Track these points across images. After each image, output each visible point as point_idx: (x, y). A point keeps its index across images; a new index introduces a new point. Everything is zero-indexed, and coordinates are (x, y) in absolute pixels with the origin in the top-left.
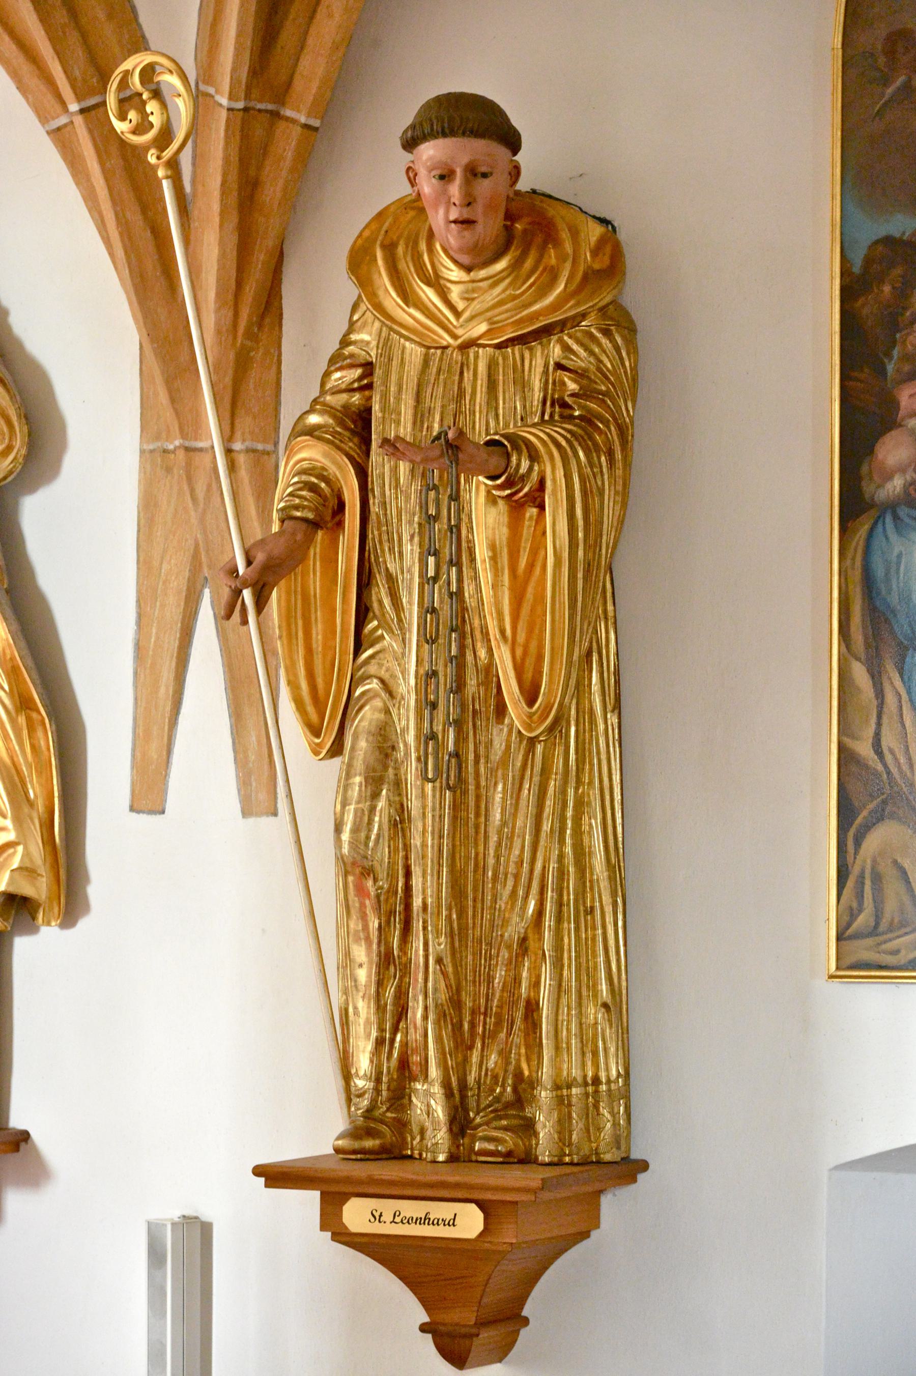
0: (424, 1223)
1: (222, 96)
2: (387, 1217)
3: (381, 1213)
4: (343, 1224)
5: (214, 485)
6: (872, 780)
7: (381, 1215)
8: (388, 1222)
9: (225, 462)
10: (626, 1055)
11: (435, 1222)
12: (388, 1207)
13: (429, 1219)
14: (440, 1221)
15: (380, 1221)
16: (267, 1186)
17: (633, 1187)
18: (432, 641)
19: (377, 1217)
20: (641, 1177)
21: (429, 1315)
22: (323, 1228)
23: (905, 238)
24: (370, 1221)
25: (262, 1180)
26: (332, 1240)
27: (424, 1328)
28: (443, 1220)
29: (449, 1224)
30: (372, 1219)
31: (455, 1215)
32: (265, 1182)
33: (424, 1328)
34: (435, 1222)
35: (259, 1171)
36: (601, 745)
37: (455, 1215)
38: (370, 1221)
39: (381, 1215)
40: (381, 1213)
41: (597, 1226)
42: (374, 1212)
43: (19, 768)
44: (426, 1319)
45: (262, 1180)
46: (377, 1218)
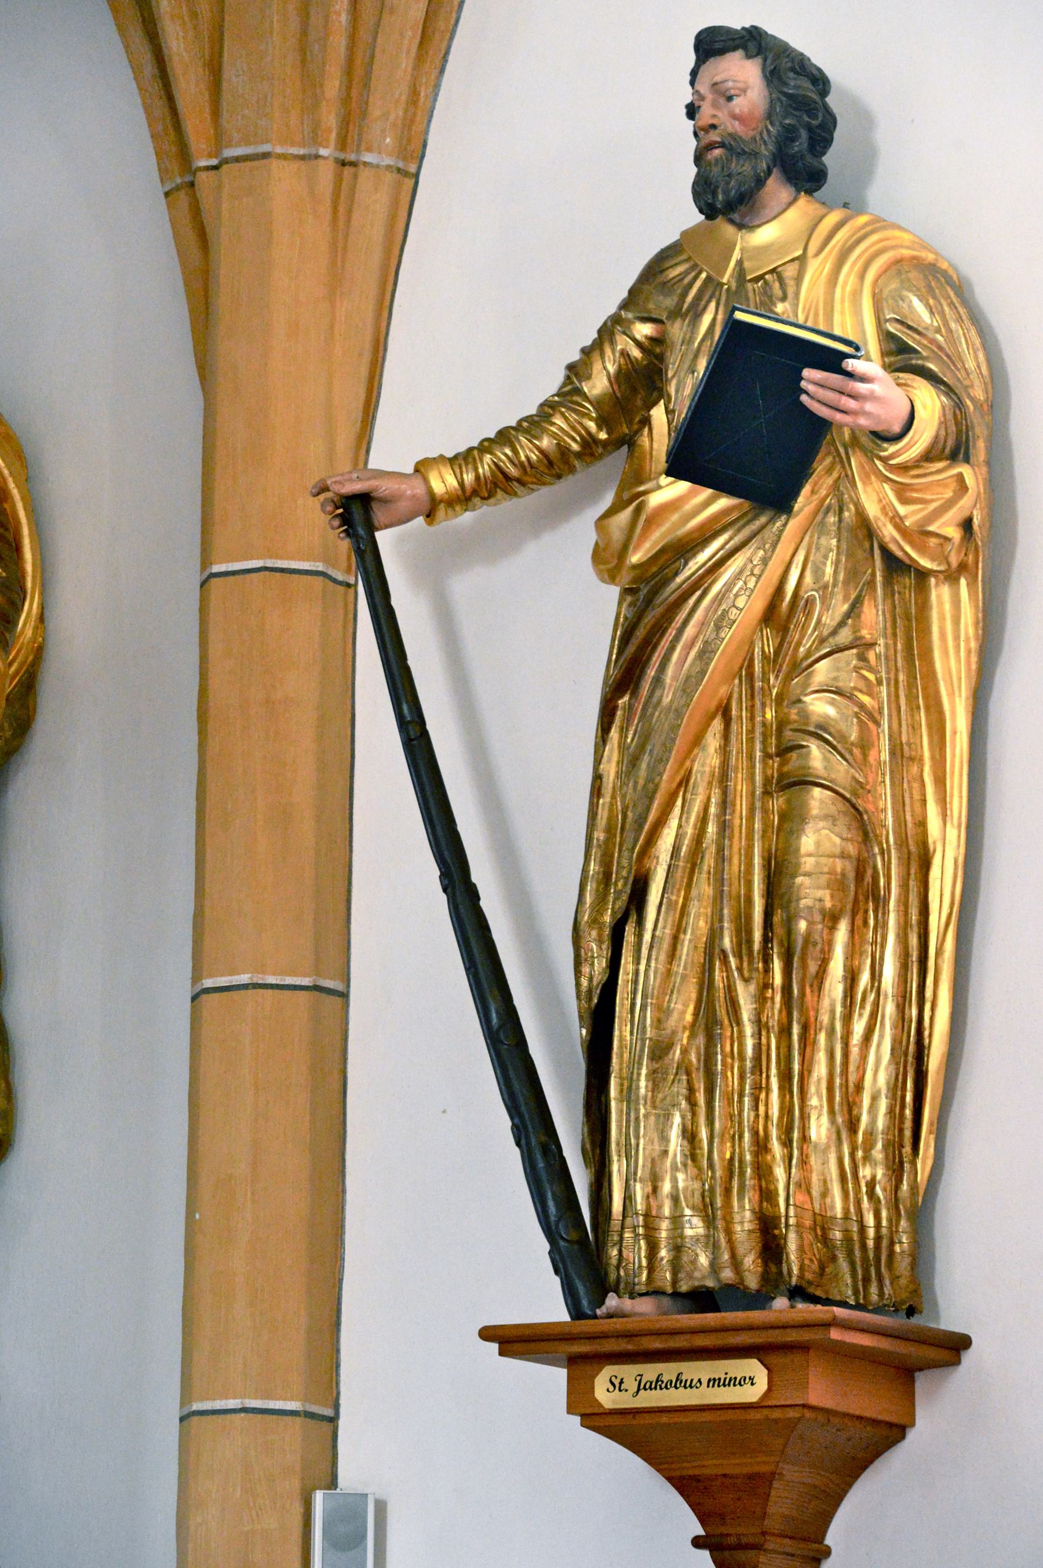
1: (868, 359)
2: (631, 1385)
3: (622, 1379)
6: (769, 483)
7: (621, 1382)
9: (970, 724)
11: (647, 1386)
14: (747, 1380)
15: (620, 1390)
16: (501, 1353)
22: (571, 1410)
24: (608, 1390)
25: (495, 1347)
26: (582, 1425)
27: (698, 1543)
28: (750, 1378)
29: (666, 1387)
30: (611, 1388)
33: (698, 1543)
34: (647, 1386)
35: (487, 1334)
38: (608, 1390)
39: (621, 1382)
40: (622, 1379)
42: (613, 1379)
44: (701, 1532)
45: (495, 1347)
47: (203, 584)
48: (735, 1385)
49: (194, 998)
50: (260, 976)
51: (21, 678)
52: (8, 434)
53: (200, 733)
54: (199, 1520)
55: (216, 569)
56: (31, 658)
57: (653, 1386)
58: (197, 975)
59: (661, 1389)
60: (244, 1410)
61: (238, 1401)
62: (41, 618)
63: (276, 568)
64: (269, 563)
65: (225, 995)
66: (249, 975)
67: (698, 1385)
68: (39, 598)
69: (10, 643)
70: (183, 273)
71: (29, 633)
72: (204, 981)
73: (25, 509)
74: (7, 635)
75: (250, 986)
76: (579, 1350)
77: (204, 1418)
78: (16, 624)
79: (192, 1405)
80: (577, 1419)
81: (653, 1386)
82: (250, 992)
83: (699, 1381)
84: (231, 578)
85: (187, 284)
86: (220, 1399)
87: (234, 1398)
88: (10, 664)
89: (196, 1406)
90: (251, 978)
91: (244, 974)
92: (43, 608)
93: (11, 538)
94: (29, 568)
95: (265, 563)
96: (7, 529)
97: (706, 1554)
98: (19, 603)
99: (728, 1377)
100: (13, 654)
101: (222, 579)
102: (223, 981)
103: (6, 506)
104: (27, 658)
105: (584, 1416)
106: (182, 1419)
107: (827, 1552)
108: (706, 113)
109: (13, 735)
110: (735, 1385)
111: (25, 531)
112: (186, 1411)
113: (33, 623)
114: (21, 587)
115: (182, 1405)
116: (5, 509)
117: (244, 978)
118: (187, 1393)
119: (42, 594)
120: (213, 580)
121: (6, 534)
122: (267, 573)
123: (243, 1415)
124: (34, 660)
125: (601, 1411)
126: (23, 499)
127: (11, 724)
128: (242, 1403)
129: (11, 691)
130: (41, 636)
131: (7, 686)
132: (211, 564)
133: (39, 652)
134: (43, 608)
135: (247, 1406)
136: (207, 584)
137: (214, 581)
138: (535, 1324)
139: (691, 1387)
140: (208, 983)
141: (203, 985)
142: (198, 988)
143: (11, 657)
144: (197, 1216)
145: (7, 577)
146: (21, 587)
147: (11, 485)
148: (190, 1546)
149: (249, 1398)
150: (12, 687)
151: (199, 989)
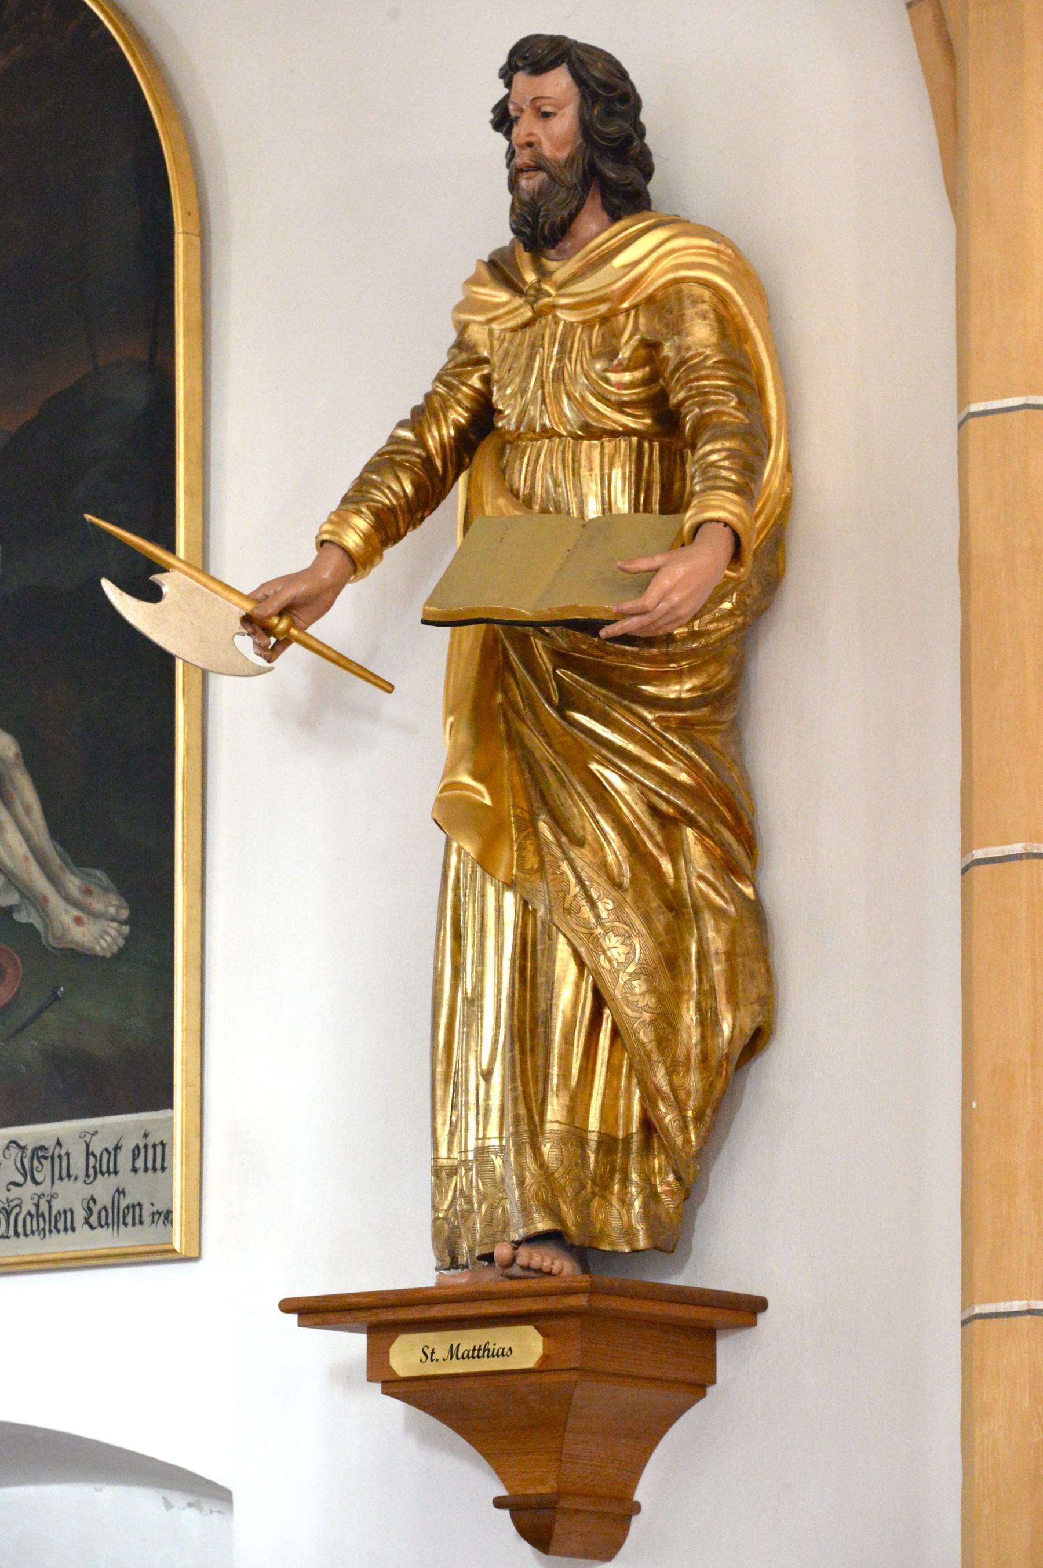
0: (483, 1356)
2: (442, 1352)
4: (391, 1368)
5: (646, 792)
7: (433, 1353)
8: (441, 1360)
10: (369, 676)
12: (469, 1339)
13: (489, 1350)
15: (432, 1360)
17: (753, 1330)
18: (562, 873)
19: (429, 1355)
20: (761, 1318)
21: (508, 1488)
23: (125, 914)
27: (499, 1503)
31: (389, 688)
32: (299, 1320)
33: (499, 1503)
35: (287, 1306)
36: (592, 807)
37: (389, 688)
39: (433, 1353)
41: (713, 1382)
43: (692, 533)
44: (503, 1492)
45: (294, 1317)
46: (429, 1355)
47: (961, 425)
48: (488, 1357)
49: (965, 870)
50: (1035, 845)
51: (768, 532)
52: (747, 271)
53: (962, 588)
54: (985, 1430)
55: (974, 408)
56: (778, 510)
57: (470, 1355)
58: (967, 846)
59: (488, 1357)
60: (1030, 1312)
61: (1024, 1302)
62: (789, 467)
63: (1039, 405)
64: (1032, 400)
65: (998, 865)
66: (1023, 844)
67: (509, 1353)
68: (785, 445)
69: (755, 493)
70: (929, 91)
71: (776, 482)
72: (974, 852)
73: (767, 351)
74: (752, 486)
75: (1024, 857)
76: (389, 1318)
77: (988, 1321)
78: (761, 474)
79: (973, 1308)
80: (378, 1386)
81: (470, 1355)
82: (1024, 862)
83: (510, 1349)
84: (990, 417)
85: (933, 99)
86: (1004, 1300)
87: (1020, 1299)
88: (757, 517)
89: (978, 1309)
90: (1025, 848)
91: (1016, 843)
92: (789, 455)
93: (753, 381)
94: (773, 413)
95: (1027, 400)
96: (749, 373)
97: (506, 1514)
98: (764, 451)
99: (497, 1348)
100: (760, 505)
101: (981, 418)
102: (995, 852)
103: (747, 347)
104: (773, 513)
105: (384, 1382)
106: (964, 1323)
107: (636, 1508)
108: (526, 126)
109: (760, 593)
110: (458, 1358)
111: (768, 373)
112: (967, 1314)
113: (779, 472)
114: (765, 434)
115: (963, 1309)
116: (746, 351)
117: (1017, 848)
118: (968, 1293)
119: (789, 441)
120: (971, 421)
121: (748, 378)
122: (1030, 411)
123: (1029, 1317)
124: (781, 513)
125: (397, 1378)
126: (764, 339)
127: (759, 583)
128: (1028, 1305)
129: (759, 546)
130: (788, 486)
131: (753, 541)
132: (969, 403)
133: (787, 503)
134: (789, 455)
135: (1034, 1307)
136: (966, 424)
137: (971, 421)
138: (406, 1290)
139: (503, 1355)
140: (979, 854)
141: (973, 855)
142: (968, 860)
143: (757, 509)
144: (974, 1104)
145: (750, 425)
146: (765, 434)
147: (752, 324)
148: (977, 1459)
149: (1036, 1299)
150: (758, 542)
151: (969, 861)
